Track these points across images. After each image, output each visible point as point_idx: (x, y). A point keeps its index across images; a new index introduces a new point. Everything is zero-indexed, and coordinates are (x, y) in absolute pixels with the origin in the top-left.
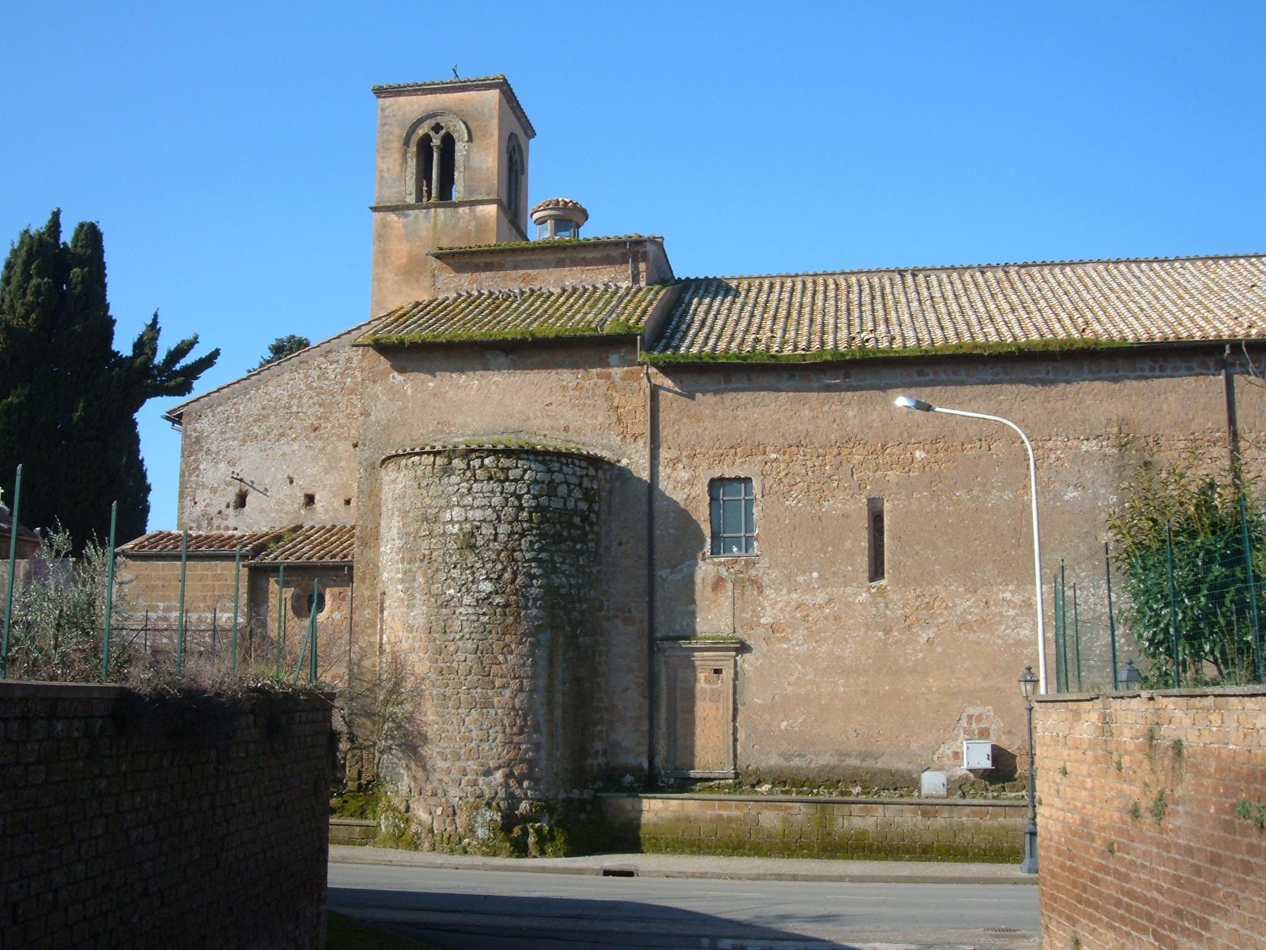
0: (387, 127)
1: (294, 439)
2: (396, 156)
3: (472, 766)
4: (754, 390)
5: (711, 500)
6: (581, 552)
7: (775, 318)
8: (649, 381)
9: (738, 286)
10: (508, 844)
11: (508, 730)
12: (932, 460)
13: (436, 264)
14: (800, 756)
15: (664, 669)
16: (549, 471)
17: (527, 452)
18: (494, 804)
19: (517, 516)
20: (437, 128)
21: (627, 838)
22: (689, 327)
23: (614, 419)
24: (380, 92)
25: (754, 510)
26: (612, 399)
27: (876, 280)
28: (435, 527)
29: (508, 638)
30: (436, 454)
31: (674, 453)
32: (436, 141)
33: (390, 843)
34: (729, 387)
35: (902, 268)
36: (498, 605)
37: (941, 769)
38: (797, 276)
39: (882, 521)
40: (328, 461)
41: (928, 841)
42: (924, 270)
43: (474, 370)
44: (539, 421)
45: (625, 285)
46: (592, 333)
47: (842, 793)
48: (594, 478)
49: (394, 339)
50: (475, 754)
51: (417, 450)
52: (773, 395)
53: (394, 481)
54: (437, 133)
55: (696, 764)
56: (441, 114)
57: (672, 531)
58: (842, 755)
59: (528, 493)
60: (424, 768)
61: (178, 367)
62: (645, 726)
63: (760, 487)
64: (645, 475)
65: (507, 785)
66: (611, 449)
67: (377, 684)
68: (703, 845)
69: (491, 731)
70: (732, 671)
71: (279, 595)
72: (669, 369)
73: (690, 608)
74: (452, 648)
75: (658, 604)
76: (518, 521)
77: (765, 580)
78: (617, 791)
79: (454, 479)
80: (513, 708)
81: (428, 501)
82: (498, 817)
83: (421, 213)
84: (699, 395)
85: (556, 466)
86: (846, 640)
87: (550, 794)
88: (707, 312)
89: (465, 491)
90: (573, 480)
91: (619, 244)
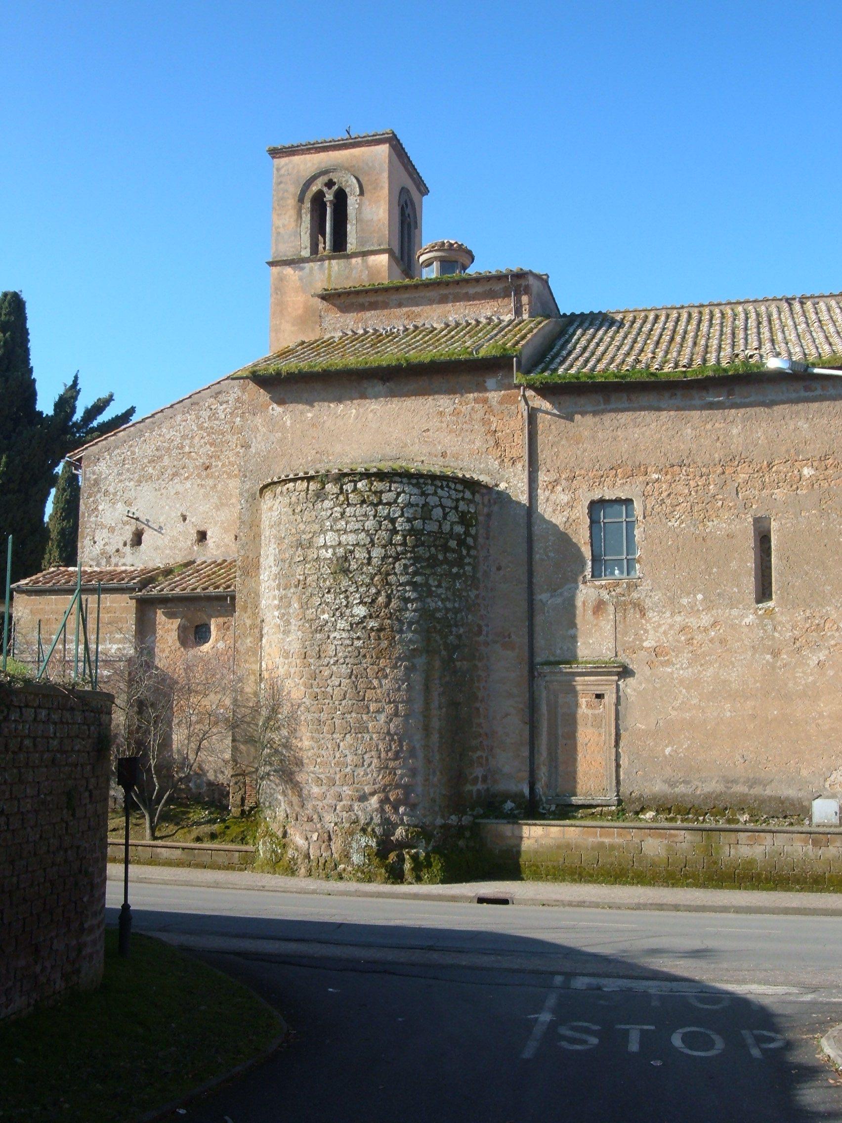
0: (282, 186)
1: (187, 478)
2: (292, 213)
3: (347, 791)
4: (634, 410)
5: (592, 522)
6: (457, 576)
7: (658, 343)
8: (527, 404)
9: (623, 319)
10: (383, 871)
11: (383, 755)
12: (821, 477)
13: (321, 305)
14: (686, 782)
15: (544, 694)
16: (423, 494)
17: (400, 475)
18: (369, 829)
19: (391, 540)
20: (330, 184)
21: (508, 866)
22: (570, 353)
23: (492, 443)
24: (275, 153)
25: (636, 532)
26: (490, 423)
27: (763, 308)
28: (309, 552)
29: (382, 663)
30: (310, 479)
31: (553, 476)
32: (329, 197)
33: (266, 868)
34: (609, 407)
35: (790, 296)
36: (372, 629)
37: (833, 796)
38: (682, 307)
39: (770, 541)
40: (220, 498)
41: (820, 871)
42: (812, 297)
43: (352, 399)
44: (417, 447)
45: (507, 318)
46: (468, 356)
47: (729, 821)
48: (471, 501)
49: (271, 370)
50: (350, 779)
51: (291, 476)
52: (654, 415)
53: (271, 509)
54: (330, 188)
55: (578, 791)
56: (334, 170)
57: (551, 554)
58: (730, 781)
59: (402, 515)
60: (300, 796)
61: (95, 424)
62: (526, 753)
63: (642, 508)
64: (524, 499)
65: (382, 810)
66: (489, 473)
67: (256, 710)
68: (584, 873)
69: (366, 757)
70: (614, 696)
71: (167, 629)
72: (546, 390)
73: (571, 632)
74: (326, 673)
75: (538, 629)
76: (391, 544)
77: (648, 603)
78: (497, 818)
79: (327, 504)
80: (388, 733)
81: (302, 526)
82: (373, 843)
83: (316, 266)
84: (578, 417)
85: (430, 489)
86: (732, 663)
87: (427, 821)
88: (589, 341)
89: (339, 515)
90: (448, 503)
91: (500, 278)
